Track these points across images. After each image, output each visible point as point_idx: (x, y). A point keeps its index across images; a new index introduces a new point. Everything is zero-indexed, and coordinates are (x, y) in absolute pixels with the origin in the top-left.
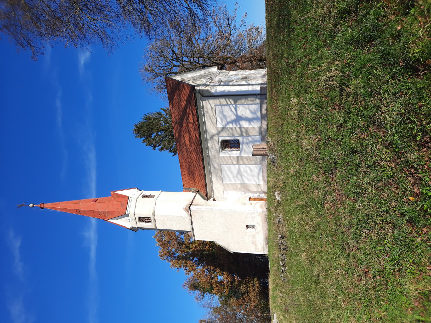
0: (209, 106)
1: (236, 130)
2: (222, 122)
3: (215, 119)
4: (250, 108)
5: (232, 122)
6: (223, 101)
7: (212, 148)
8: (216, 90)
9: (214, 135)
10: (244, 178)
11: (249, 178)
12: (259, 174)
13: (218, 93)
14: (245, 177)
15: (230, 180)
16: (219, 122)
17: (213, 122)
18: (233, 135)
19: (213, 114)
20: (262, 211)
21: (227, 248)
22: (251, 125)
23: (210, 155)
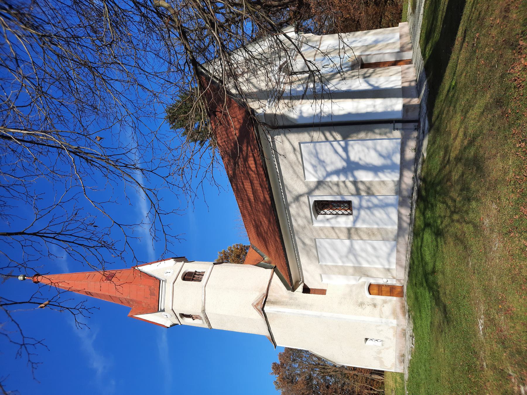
0: (287, 145)
1: (346, 186)
2: (316, 171)
3: (301, 168)
4: (379, 148)
5: (337, 172)
6: (317, 135)
7: (298, 214)
8: (301, 112)
9: (301, 195)
10: (360, 259)
11: (369, 259)
12: (389, 255)
13: (306, 118)
14: (362, 257)
15: (334, 261)
16: (311, 173)
17: (298, 172)
18: (340, 194)
19: (297, 159)
20: (398, 325)
21: (304, 123)
22: (379, 177)
23: (294, 224)
